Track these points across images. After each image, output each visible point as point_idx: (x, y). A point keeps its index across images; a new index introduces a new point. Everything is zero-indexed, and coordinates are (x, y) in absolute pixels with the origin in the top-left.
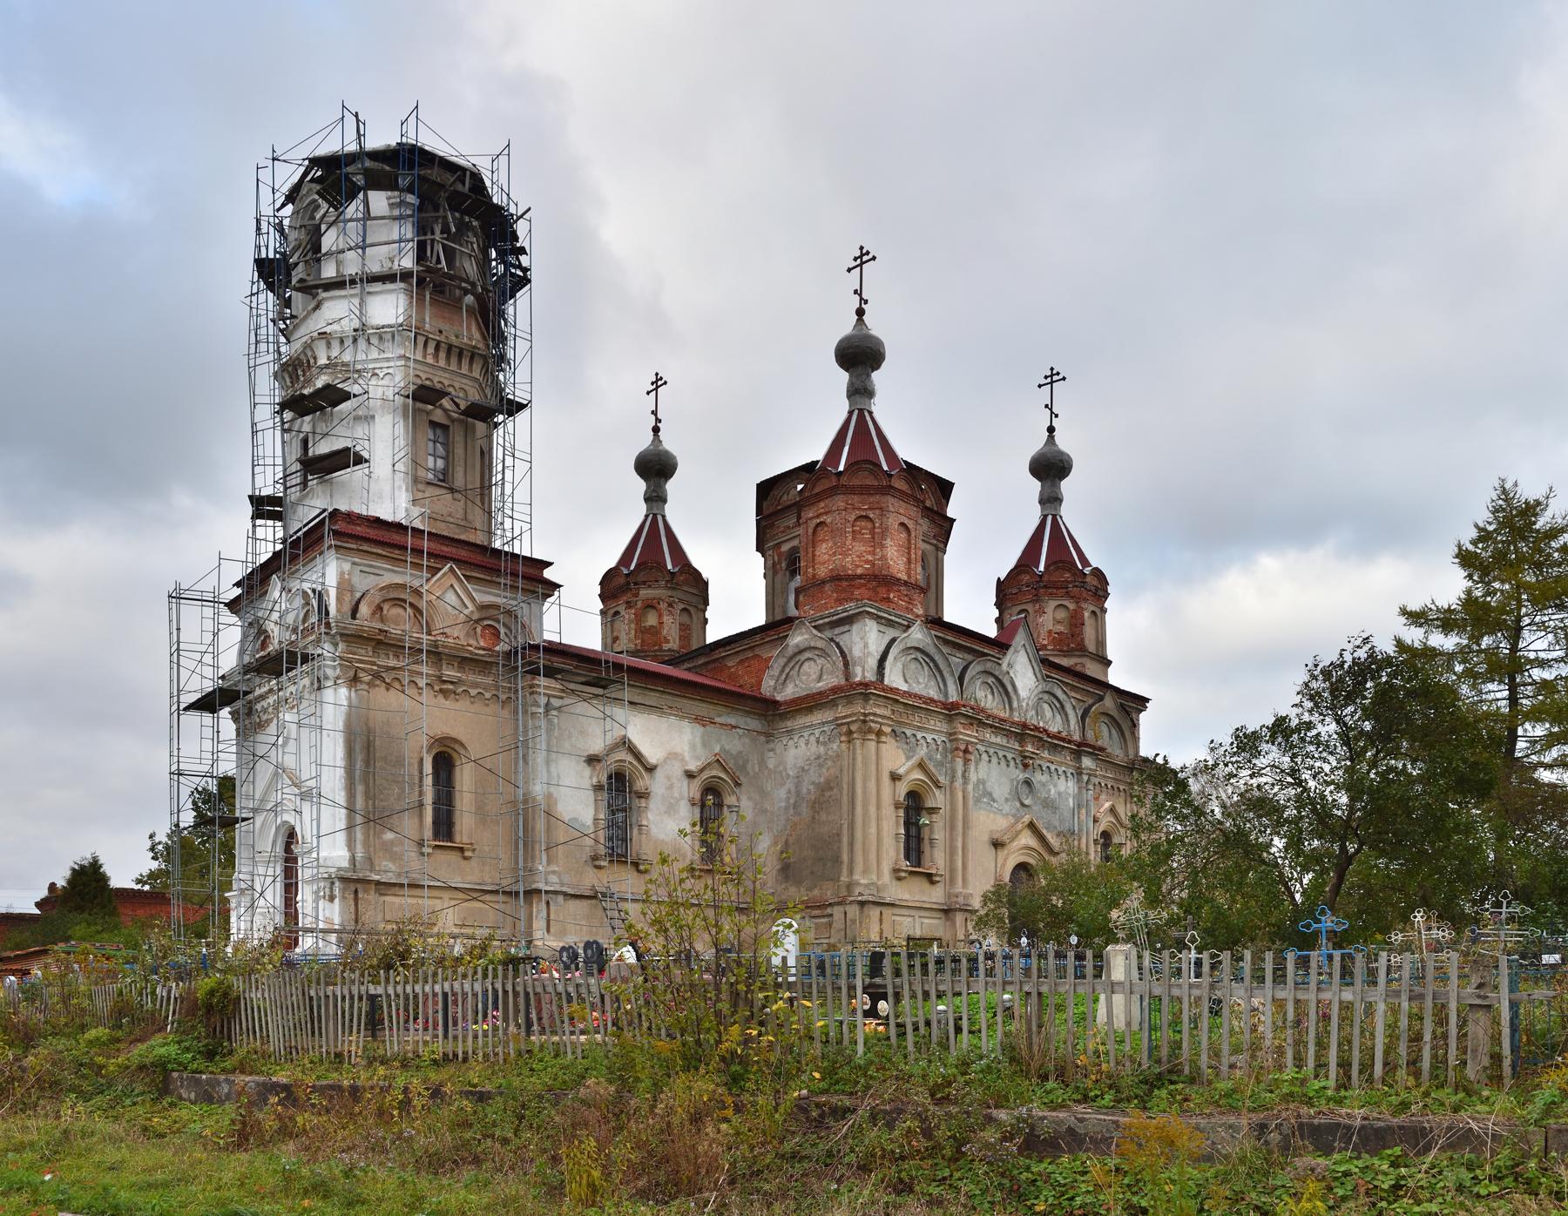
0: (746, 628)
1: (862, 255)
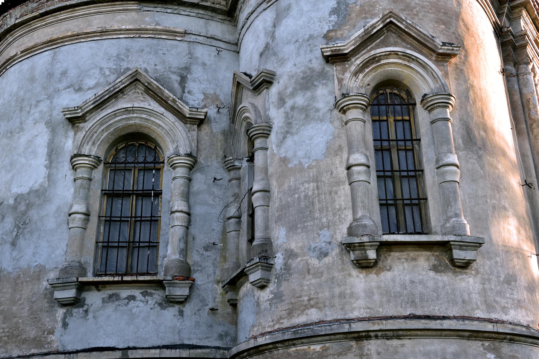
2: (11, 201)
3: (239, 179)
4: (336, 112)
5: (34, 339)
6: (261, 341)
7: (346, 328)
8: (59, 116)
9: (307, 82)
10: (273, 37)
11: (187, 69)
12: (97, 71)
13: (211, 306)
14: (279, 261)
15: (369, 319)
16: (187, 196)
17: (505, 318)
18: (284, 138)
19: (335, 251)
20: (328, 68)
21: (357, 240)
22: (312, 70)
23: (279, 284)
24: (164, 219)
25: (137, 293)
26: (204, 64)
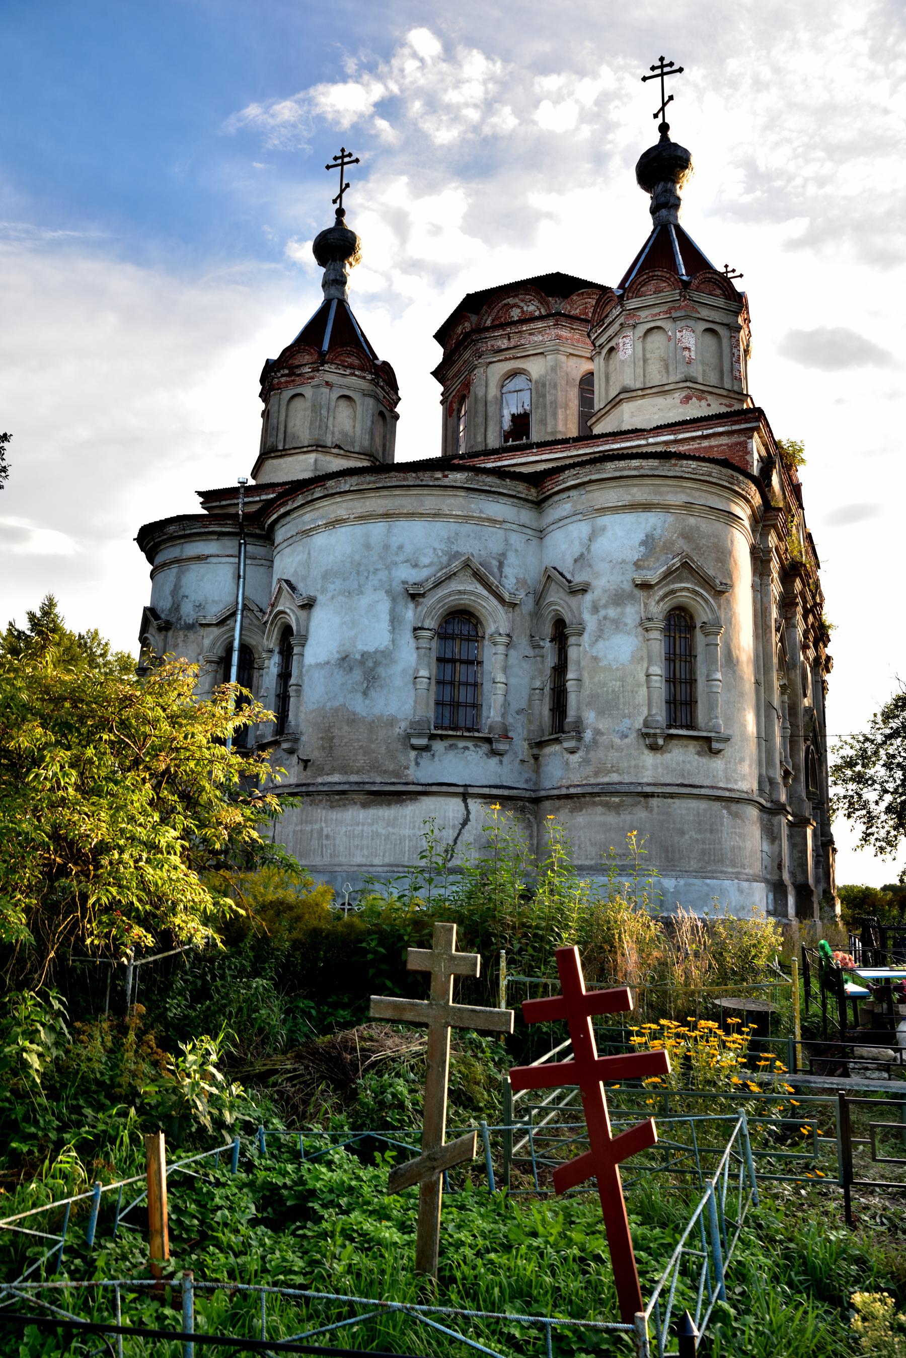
0: (168, 516)
1: (343, 157)
2: (358, 657)
3: (542, 657)
4: (640, 629)
5: (393, 771)
6: (572, 791)
7: (639, 789)
8: (398, 588)
9: (619, 599)
10: (588, 549)
11: (504, 555)
12: (431, 551)
13: (521, 757)
14: (588, 735)
15: (654, 785)
16: (505, 669)
17: (735, 787)
18: (597, 640)
19: (633, 736)
20: (637, 592)
21: (652, 731)
22: (623, 590)
23: (588, 752)
24: (487, 686)
25: (470, 744)
26: (516, 551)
